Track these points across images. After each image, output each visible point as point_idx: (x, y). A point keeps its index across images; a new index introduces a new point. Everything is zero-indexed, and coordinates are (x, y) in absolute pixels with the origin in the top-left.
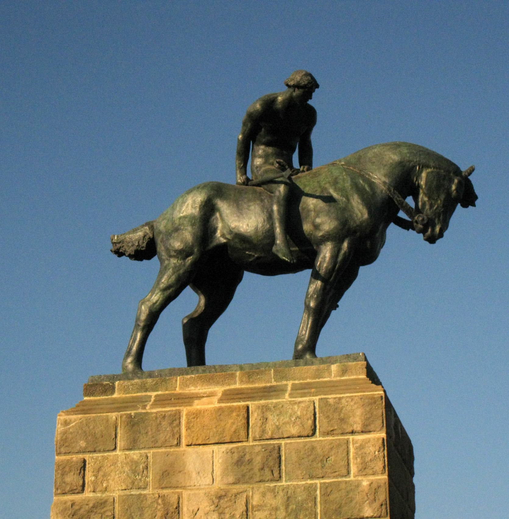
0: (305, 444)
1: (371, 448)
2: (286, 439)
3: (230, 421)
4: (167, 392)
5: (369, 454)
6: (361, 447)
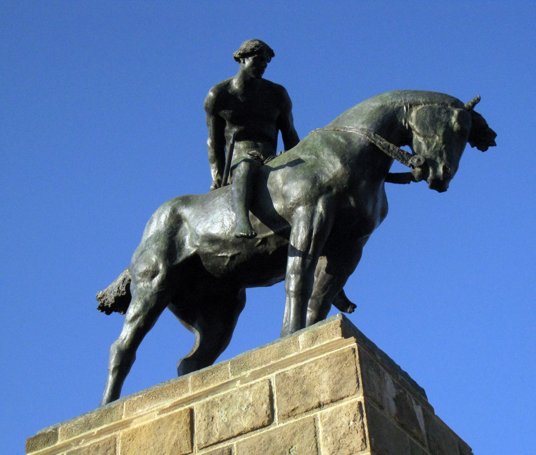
0: (261, 437)
1: (343, 419)
2: (238, 438)
3: (170, 432)
4: (112, 424)
5: (341, 426)
6: (331, 421)
